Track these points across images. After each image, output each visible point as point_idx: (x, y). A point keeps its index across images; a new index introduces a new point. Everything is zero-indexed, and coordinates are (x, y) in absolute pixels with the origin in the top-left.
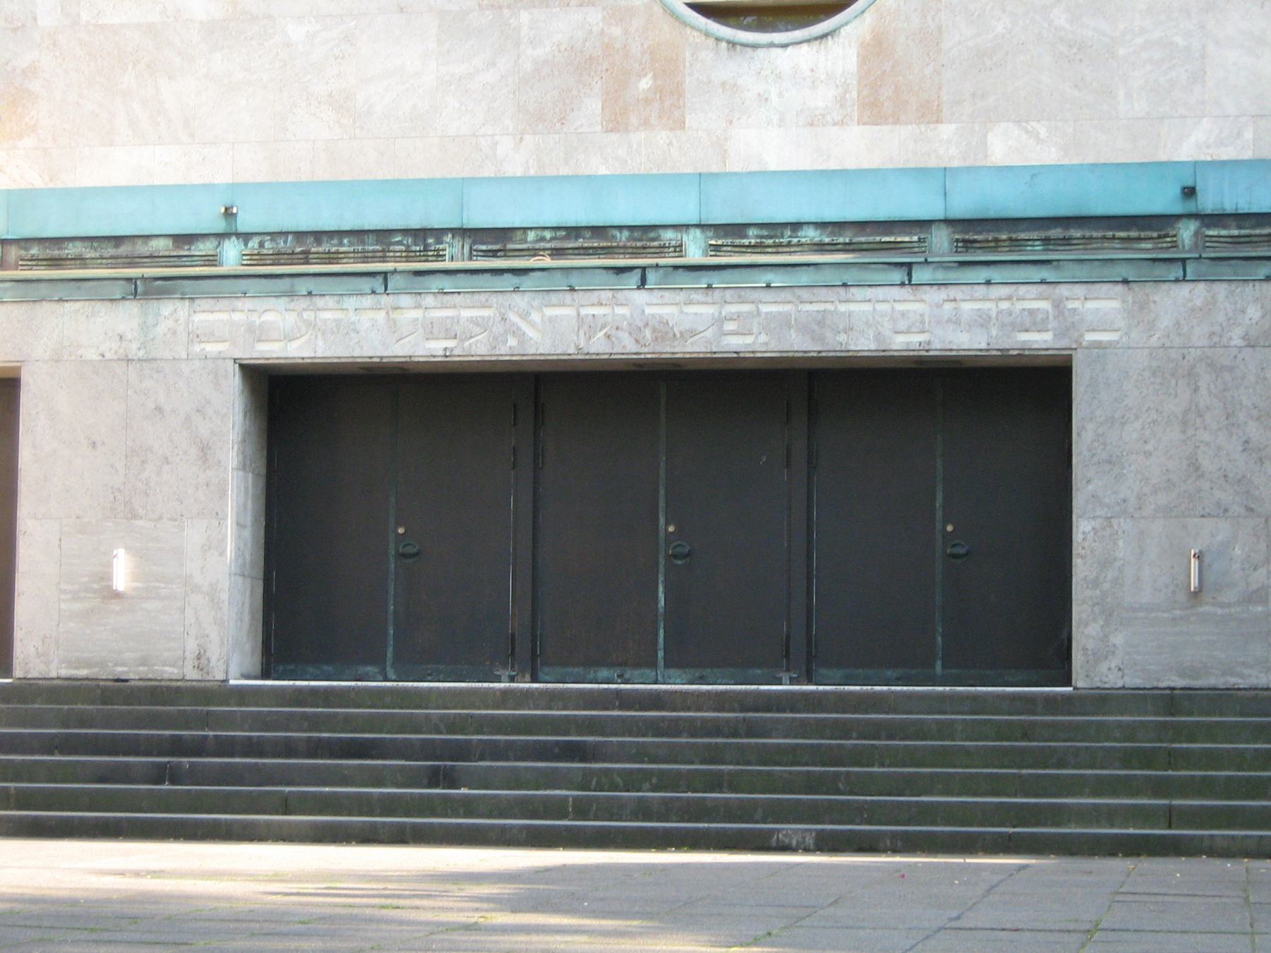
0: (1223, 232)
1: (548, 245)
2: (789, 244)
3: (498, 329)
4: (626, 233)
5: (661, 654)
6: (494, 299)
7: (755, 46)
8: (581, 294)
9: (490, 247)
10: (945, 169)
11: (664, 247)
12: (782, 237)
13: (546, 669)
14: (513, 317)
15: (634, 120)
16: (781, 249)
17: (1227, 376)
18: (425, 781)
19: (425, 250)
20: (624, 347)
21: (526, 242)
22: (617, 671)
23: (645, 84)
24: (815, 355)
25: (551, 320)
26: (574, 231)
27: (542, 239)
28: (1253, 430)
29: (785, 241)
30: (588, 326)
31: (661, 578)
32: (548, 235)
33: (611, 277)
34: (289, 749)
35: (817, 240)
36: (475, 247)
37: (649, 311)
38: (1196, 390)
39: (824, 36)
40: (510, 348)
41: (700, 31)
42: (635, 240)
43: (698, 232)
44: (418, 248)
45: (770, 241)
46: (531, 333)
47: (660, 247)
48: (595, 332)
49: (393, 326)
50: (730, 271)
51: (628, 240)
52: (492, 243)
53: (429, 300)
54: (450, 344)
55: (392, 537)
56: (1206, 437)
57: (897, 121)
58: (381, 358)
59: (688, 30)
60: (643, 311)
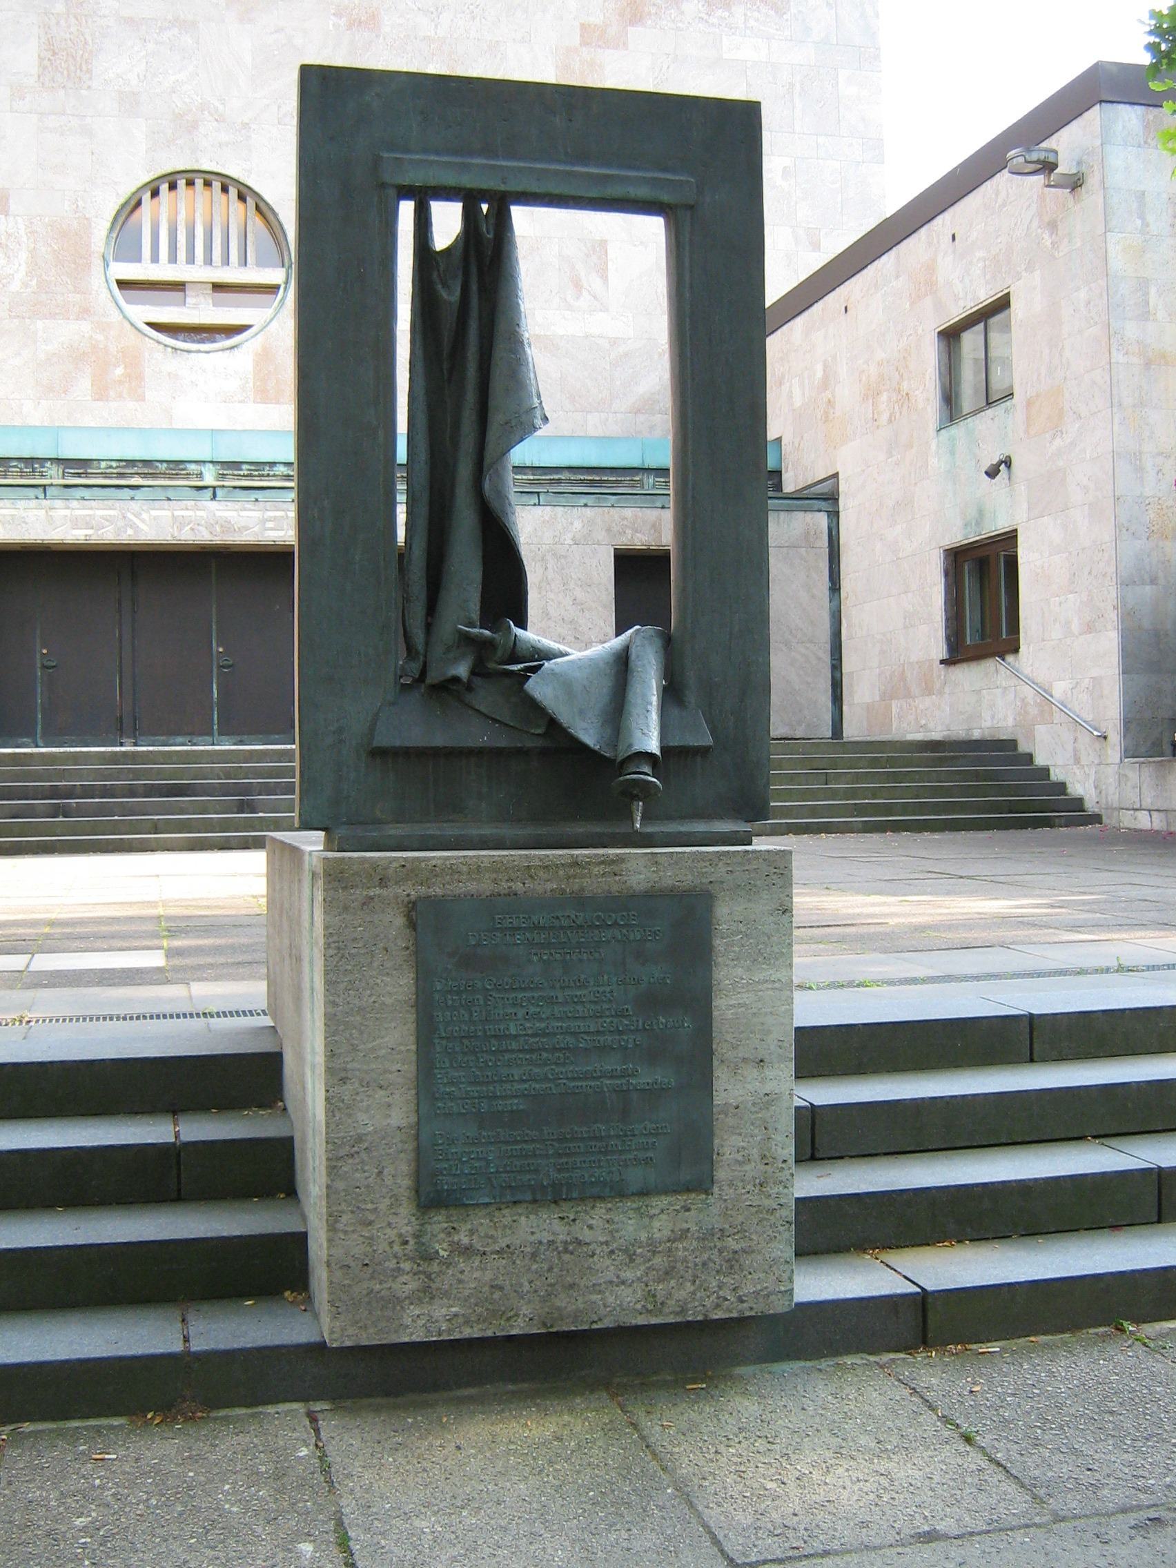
0: (524, 477)
1: (115, 471)
2: (268, 475)
3: (121, 523)
4: (165, 465)
5: (215, 727)
6: (117, 504)
7: (189, 351)
8: (175, 502)
9: (76, 471)
10: (212, 430)
11: (190, 474)
12: (264, 470)
13: (142, 738)
14: (130, 516)
15: (112, 394)
16: (263, 478)
17: (563, 561)
18: (235, 810)
19: (33, 472)
20: (203, 536)
21: (100, 469)
22: (189, 738)
23: (119, 371)
24: (191, 542)
25: (155, 518)
26: (131, 463)
27: (111, 467)
28: (579, 594)
29: (265, 473)
30: (180, 522)
31: (215, 680)
32: (114, 464)
33: (194, 493)
34: (131, 791)
35: (285, 473)
36: (67, 471)
37: (218, 514)
38: (546, 568)
39: (232, 348)
40: (129, 535)
41: (154, 340)
42: (172, 469)
43: (211, 466)
44: (28, 470)
45: (256, 473)
46: (141, 525)
47: (187, 474)
48: (184, 526)
49: (50, 519)
50: (268, 490)
51: (166, 469)
52: (77, 469)
53: (75, 504)
54: (90, 532)
55: (38, 656)
56: (552, 596)
57: (278, 403)
58: (43, 540)
59: (147, 339)
60: (214, 514)
